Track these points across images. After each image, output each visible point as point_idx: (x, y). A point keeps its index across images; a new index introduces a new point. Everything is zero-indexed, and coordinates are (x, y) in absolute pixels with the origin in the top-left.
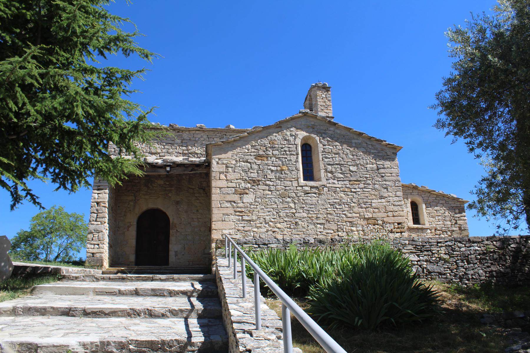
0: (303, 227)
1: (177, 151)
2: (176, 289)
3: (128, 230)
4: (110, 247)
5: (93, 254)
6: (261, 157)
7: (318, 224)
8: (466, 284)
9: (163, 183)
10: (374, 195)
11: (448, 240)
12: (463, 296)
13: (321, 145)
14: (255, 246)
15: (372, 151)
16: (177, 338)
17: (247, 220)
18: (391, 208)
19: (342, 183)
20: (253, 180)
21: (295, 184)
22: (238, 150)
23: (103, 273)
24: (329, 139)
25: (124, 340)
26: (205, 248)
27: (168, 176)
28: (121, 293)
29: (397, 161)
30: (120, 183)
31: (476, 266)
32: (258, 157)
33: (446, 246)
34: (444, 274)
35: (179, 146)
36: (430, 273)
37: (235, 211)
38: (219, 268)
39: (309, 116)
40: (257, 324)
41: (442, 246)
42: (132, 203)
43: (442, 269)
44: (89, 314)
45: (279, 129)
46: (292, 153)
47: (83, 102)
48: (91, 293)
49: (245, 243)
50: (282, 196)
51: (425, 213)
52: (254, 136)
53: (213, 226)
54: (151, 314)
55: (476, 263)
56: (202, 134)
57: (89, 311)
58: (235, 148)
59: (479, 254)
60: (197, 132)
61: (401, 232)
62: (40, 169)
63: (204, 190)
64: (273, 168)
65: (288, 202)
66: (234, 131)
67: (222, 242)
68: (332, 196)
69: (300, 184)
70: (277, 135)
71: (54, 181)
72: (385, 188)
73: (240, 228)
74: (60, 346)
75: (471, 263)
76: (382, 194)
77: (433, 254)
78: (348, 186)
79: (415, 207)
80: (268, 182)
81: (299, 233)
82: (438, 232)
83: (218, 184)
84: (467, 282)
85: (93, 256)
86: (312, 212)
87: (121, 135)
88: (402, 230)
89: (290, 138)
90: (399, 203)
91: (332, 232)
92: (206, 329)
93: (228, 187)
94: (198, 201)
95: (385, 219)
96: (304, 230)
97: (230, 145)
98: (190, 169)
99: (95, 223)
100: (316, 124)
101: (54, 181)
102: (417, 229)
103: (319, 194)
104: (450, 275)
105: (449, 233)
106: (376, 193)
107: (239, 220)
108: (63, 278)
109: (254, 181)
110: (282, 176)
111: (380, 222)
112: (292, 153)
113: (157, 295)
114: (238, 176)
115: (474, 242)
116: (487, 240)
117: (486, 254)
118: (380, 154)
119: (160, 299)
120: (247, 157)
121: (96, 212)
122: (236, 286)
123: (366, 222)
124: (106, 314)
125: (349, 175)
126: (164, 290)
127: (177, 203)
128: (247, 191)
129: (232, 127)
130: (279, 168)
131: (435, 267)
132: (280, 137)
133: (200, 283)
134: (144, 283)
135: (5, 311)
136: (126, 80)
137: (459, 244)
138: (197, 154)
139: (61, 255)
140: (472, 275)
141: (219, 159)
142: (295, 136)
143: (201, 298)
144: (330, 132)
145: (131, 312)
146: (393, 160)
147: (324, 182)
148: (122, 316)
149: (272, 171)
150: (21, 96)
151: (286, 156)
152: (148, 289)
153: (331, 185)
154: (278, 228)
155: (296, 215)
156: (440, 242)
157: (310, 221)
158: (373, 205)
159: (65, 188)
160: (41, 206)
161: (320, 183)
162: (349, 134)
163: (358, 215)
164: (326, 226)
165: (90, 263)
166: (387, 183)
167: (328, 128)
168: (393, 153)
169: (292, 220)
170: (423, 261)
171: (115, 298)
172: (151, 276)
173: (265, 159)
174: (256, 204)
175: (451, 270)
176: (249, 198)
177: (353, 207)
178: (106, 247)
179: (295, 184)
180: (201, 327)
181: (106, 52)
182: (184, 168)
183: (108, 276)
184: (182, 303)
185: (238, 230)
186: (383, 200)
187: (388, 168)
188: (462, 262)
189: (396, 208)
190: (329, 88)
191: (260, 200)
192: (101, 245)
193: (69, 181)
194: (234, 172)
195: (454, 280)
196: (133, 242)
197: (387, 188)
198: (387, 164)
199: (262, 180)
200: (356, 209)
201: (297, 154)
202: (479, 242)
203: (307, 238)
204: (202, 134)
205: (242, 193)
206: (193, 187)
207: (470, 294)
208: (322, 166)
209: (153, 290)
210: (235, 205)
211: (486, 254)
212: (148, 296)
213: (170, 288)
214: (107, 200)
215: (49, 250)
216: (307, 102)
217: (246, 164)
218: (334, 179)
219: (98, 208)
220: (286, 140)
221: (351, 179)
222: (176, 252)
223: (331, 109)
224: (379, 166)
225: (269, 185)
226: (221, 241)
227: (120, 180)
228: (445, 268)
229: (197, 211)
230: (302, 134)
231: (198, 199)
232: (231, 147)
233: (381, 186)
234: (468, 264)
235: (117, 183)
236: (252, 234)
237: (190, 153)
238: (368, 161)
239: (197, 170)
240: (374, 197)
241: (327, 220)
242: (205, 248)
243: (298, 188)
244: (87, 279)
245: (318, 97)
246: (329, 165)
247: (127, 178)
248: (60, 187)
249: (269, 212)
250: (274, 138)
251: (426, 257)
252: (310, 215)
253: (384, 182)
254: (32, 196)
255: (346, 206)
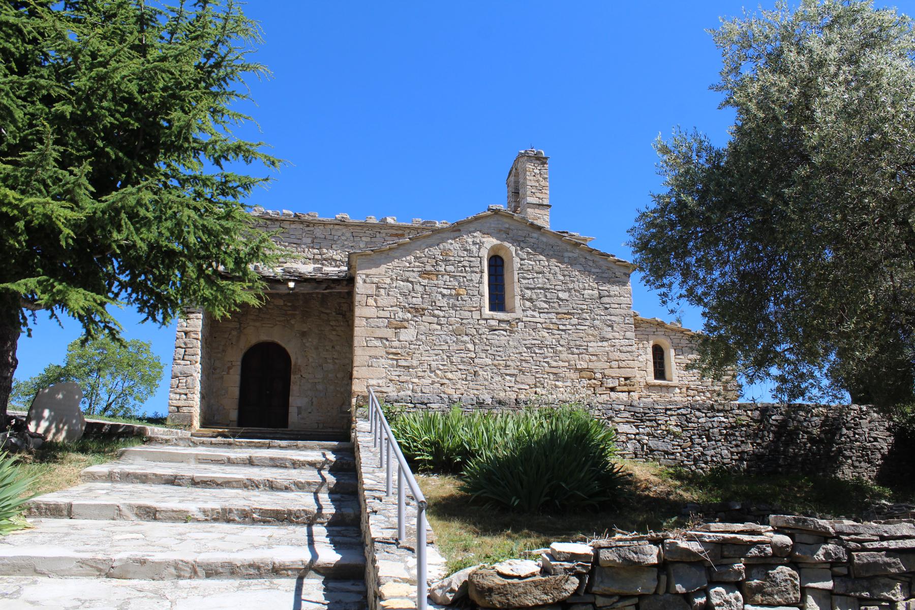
0: (486, 379)
1: (305, 255)
2: (302, 459)
3: (228, 373)
4: (203, 397)
5: (178, 407)
6: (429, 274)
7: (507, 375)
8: (702, 469)
9: (282, 304)
10: (592, 335)
11: (681, 406)
12: (678, 483)
13: (517, 259)
14: (410, 405)
15: (593, 270)
16: (305, 508)
17: (404, 367)
18: (617, 355)
19: (546, 316)
20: (415, 308)
21: (476, 315)
22: (396, 262)
23: (192, 435)
24: (530, 251)
25: (247, 508)
26: (343, 404)
27: (292, 296)
28: (230, 462)
29: (629, 286)
30: (228, 315)
31: (720, 444)
32: (424, 274)
33: (678, 414)
34: (673, 454)
35: (309, 247)
36: (652, 451)
37: (388, 353)
38: (358, 434)
39: (502, 215)
40: (387, 492)
41: (672, 415)
42: (234, 333)
43: (670, 447)
44: (198, 483)
45: (456, 234)
46: (475, 269)
47: (195, 226)
48: (192, 460)
49: (397, 401)
50: (457, 333)
51: (673, 363)
52: (419, 243)
53: (355, 373)
54: (271, 486)
55: (720, 441)
56: (344, 231)
57: (198, 480)
58: (392, 259)
59: (725, 428)
60: (337, 227)
61: (629, 392)
62: (123, 294)
63: (344, 316)
64: (445, 292)
65: (465, 342)
66: (392, 227)
67: (365, 398)
68: (529, 335)
69: (484, 317)
70: (453, 242)
71: (141, 310)
72: (609, 326)
73: (393, 377)
74: (179, 511)
75: (712, 440)
76: (604, 334)
77: (659, 425)
78: (554, 321)
79: (658, 354)
80: (436, 312)
81: (479, 387)
82: (691, 393)
83: (363, 311)
84: (703, 465)
85: (178, 411)
86: (499, 358)
87: (236, 258)
88: (631, 388)
89: (472, 247)
90: (629, 349)
91: (527, 387)
92: (338, 503)
93: (378, 318)
94: (334, 333)
95: (606, 372)
96: (486, 383)
97: (383, 256)
98: (324, 286)
99: (183, 362)
100: (512, 227)
101: (141, 310)
102: (660, 386)
103: (511, 332)
104: (681, 455)
105: (708, 395)
106: (596, 333)
107: (392, 366)
108: (150, 440)
109: (417, 310)
110: (457, 303)
111: (599, 376)
112: (475, 269)
113: (276, 466)
114: (393, 301)
115: (719, 411)
116: (739, 409)
117: (735, 427)
118: (604, 275)
119: (281, 471)
120: (407, 274)
121: (183, 346)
122: (375, 455)
123: (577, 375)
124: (218, 485)
125: (556, 305)
126: (286, 459)
127: (304, 334)
128: (406, 324)
129: (390, 220)
130: (454, 292)
131: (660, 443)
132: (457, 246)
133: (333, 453)
134: (258, 450)
135: (100, 477)
136: (245, 189)
137: (697, 413)
138: (335, 260)
139: (113, 406)
140: (712, 456)
141: (367, 276)
142: (480, 245)
143: (333, 470)
144: (532, 240)
145: (248, 483)
146: (624, 284)
147: (519, 314)
148: (237, 488)
149: (443, 295)
150: (126, 223)
151: (465, 274)
152: (265, 458)
153: (528, 319)
154: (449, 379)
155: (476, 361)
156: (670, 409)
157: (495, 371)
158: (590, 350)
159: (155, 320)
160: (121, 345)
161: (513, 315)
162: (560, 243)
163: (566, 364)
164: (518, 379)
165: (173, 420)
166: (613, 318)
167: (530, 236)
168: (625, 274)
169: (469, 368)
170: (644, 434)
171: (223, 467)
172: (267, 441)
173: (435, 278)
174: (419, 343)
175: (683, 449)
176: (408, 335)
177: (560, 351)
178: (197, 398)
179: (476, 315)
180: (332, 501)
181: (222, 161)
182: (316, 285)
183: (209, 439)
184: (311, 475)
185: (391, 380)
186: (605, 344)
187: (615, 295)
188: (700, 437)
189: (623, 356)
190: (546, 158)
191: (423, 337)
192: (189, 395)
193: (161, 311)
194: (388, 295)
195: (686, 462)
196: (235, 391)
197: (612, 326)
198: (615, 289)
199: (427, 309)
200: (564, 356)
201: (482, 272)
202: (726, 411)
203: (481, 397)
204: (344, 231)
205: (399, 327)
206: (328, 311)
207: (691, 480)
208: (517, 290)
209: (272, 459)
210: (387, 343)
211: (735, 427)
212: (265, 466)
213: (294, 458)
214: (200, 329)
215: (94, 398)
216: (512, 178)
217: (405, 283)
218: (534, 311)
219: (187, 340)
220: (466, 250)
221: (560, 310)
222: (299, 408)
223: (548, 192)
224: (603, 293)
225: (438, 317)
226: (364, 397)
227: (229, 311)
228: (673, 445)
229: (333, 347)
230: (490, 242)
231: (334, 330)
232: (386, 258)
233: (604, 322)
234: (708, 441)
235: (225, 315)
236: (411, 386)
237: (325, 260)
238: (586, 285)
239: (335, 288)
240: (592, 338)
241: (520, 370)
242: (343, 404)
243: (481, 322)
244: (181, 442)
245: (528, 173)
246: (528, 288)
247: (238, 310)
248: (147, 319)
249: (436, 355)
250: (450, 246)
251: (648, 429)
252: (496, 362)
253: (609, 317)
254: (111, 329)
255: (550, 350)
